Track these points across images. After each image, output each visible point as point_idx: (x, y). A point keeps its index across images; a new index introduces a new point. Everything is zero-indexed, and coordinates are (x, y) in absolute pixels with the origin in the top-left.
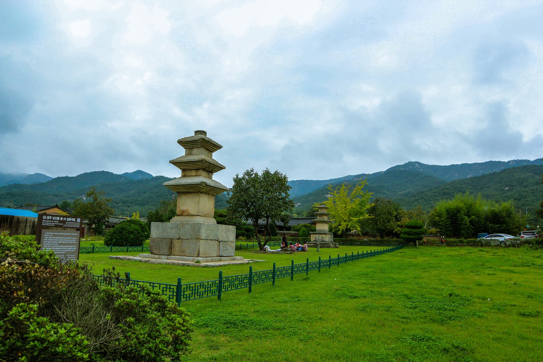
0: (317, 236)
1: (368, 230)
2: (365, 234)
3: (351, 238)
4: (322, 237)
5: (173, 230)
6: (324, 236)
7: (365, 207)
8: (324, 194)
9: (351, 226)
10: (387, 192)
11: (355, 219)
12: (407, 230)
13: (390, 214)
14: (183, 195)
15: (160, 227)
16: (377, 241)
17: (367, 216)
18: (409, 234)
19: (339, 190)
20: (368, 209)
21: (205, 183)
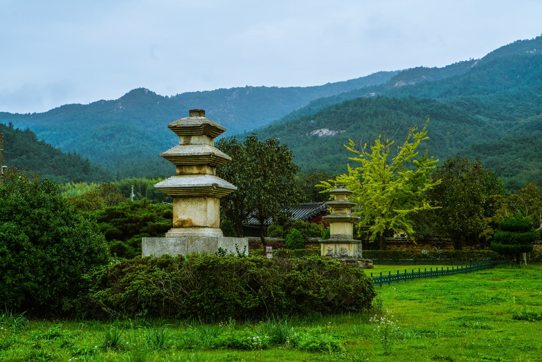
0: (332, 247)
1: (428, 230)
2: (424, 241)
3: (394, 248)
4: (342, 250)
5: (178, 248)
6: (345, 246)
7: (423, 187)
8: (312, 128)
9: (395, 226)
10: (487, 120)
11: (404, 212)
12: (502, 234)
13: (476, 201)
14: (181, 200)
15: (157, 243)
16: (449, 255)
17: (426, 206)
18: (506, 242)
19: (370, 152)
20: (429, 191)
21: (216, 185)
